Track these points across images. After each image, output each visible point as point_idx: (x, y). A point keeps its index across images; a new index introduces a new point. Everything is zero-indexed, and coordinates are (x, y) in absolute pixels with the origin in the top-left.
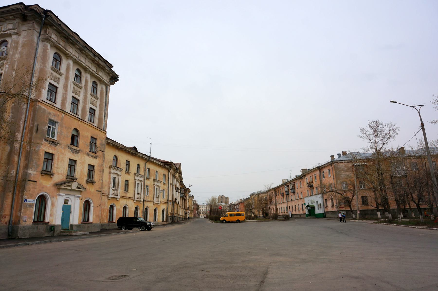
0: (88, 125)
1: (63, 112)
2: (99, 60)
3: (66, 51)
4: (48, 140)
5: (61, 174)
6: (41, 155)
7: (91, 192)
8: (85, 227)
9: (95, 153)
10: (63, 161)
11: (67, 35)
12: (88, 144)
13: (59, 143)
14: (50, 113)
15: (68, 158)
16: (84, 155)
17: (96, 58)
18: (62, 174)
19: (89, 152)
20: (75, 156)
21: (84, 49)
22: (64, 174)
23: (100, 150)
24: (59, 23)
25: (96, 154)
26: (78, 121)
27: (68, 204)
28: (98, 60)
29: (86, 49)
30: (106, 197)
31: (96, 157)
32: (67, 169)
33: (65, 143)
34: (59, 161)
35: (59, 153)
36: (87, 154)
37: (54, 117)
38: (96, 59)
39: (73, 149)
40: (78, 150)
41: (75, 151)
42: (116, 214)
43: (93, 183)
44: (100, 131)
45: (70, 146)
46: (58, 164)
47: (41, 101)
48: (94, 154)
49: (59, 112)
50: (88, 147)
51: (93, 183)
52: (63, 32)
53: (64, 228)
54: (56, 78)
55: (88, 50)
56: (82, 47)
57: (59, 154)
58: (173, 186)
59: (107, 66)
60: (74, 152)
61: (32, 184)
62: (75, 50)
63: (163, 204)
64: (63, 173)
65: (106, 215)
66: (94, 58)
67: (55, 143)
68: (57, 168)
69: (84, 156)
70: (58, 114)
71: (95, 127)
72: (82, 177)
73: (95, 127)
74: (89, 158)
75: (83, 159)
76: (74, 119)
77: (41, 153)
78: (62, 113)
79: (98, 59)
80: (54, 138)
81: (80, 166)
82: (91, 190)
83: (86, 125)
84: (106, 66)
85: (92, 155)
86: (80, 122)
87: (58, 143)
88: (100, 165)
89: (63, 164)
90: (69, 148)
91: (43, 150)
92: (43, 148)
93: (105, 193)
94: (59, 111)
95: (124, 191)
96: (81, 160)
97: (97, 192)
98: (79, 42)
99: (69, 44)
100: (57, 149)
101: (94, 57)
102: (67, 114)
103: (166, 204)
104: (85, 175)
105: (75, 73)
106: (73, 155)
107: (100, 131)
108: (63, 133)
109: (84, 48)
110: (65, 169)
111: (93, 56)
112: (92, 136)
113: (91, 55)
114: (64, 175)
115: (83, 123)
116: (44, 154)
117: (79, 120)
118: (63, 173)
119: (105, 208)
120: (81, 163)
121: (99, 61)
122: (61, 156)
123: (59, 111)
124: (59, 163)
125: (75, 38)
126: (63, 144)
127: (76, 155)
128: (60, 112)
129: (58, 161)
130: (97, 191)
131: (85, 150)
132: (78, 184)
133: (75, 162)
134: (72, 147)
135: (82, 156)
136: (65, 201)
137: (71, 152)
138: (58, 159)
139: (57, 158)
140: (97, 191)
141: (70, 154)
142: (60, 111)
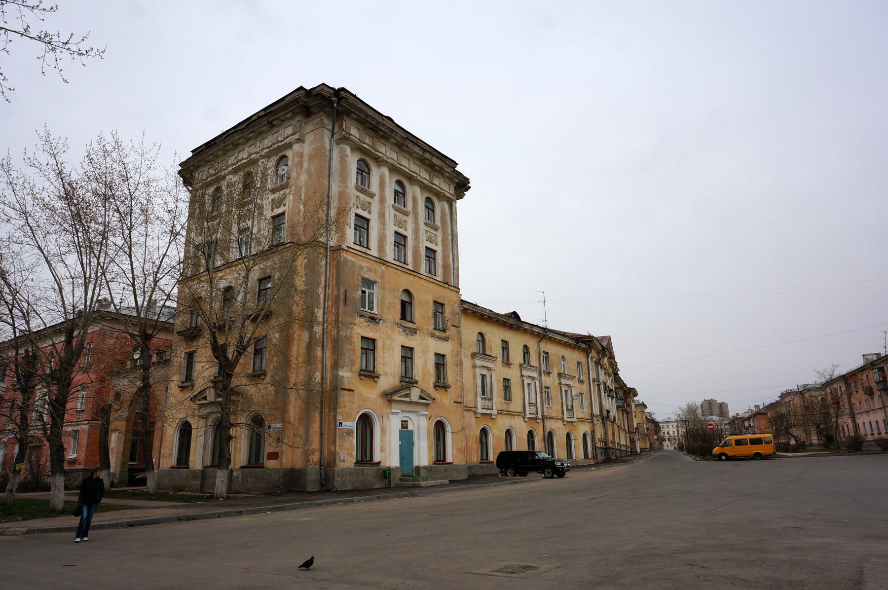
1: (382, 262)
3: (376, 153)
9: (444, 331)
14: (362, 268)
16: (425, 337)
20: (409, 340)
22: (396, 373)
23: (452, 325)
27: (408, 429)
29: (408, 141)
31: (446, 339)
34: (386, 351)
42: (493, 445)
46: (383, 357)
49: (376, 263)
52: (368, 119)
56: (401, 139)
57: (383, 338)
74: (435, 342)
78: (382, 265)
83: (422, 282)
89: (392, 358)
95: (503, 401)
97: (455, 404)
102: (389, 264)
106: (407, 338)
107: (449, 288)
114: (396, 377)
129: (384, 352)
130: (454, 402)
131: (425, 327)
136: (403, 423)
139: (381, 348)
140: (454, 402)
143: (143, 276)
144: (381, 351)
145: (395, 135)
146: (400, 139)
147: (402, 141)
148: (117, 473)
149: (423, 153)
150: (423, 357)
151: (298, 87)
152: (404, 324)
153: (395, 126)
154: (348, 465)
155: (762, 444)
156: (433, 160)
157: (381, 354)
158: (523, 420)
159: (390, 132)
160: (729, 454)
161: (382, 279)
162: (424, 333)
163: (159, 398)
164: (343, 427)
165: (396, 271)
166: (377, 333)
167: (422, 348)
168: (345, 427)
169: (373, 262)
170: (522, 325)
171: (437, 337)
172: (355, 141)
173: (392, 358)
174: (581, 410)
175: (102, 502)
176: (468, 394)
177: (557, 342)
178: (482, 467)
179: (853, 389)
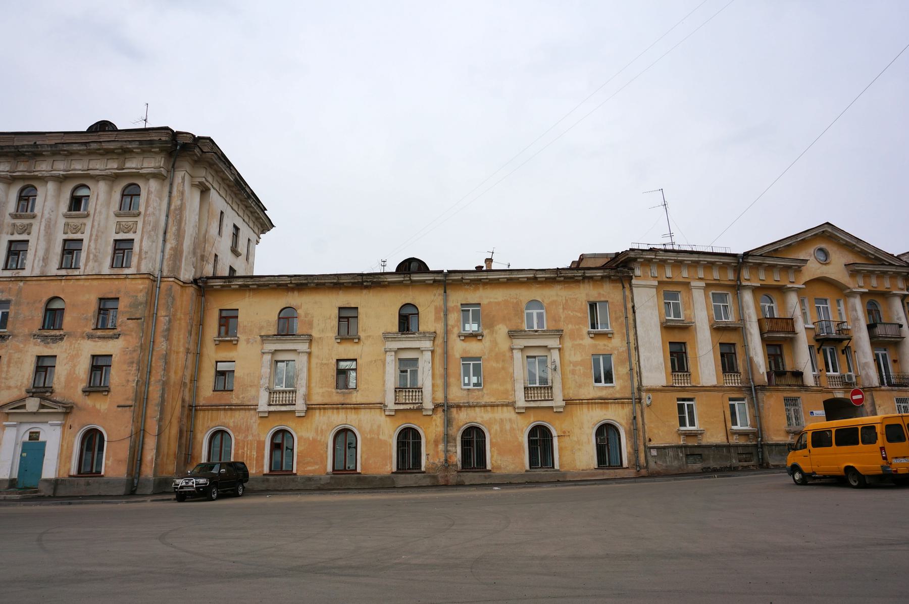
1: (19, 279)
2: (99, 144)
3: (32, 174)
7: (99, 411)
8: (78, 484)
10: (22, 363)
11: (13, 150)
12: (89, 315)
13: (10, 334)
16: (77, 340)
17: (90, 146)
19: (92, 331)
20: (51, 348)
21: (58, 149)
22: (24, 385)
23: (128, 319)
24: (30, 141)
26: (59, 281)
27: (38, 440)
28: (99, 146)
29: (60, 145)
30: (252, 412)
31: (117, 336)
32: (30, 376)
33: (27, 331)
34: (11, 365)
35: (11, 351)
38: (92, 147)
39: (47, 336)
41: (51, 339)
42: (298, 453)
43: (104, 390)
44: (127, 280)
46: (7, 371)
48: (110, 332)
50: (91, 320)
51: (104, 390)
52: (5, 150)
53: (28, 486)
54: (127, 227)
55: (65, 145)
56: (51, 147)
57: (10, 353)
59: (128, 143)
62: (142, 156)
63: (368, 410)
65: (255, 456)
66: (89, 148)
70: (10, 286)
71: (107, 277)
72: (72, 384)
73: (107, 277)
75: (74, 347)
76: (48, 282)
79: (95, 144)
82: (98, 406)
83: (81, 283)
84: (125, 143)
85: (103, 334)
87: (9, 336)
89: (20, 370)
93: (249, 403)
95: (334, 390)
96: (68, 352)
97: (120, 409)
98: (39, 146)
99: (35, 159)
100: (7, 346)
101: (86, 148)
102: (28, 279)
103: (628, 403)
104: (81, 378)
106: (46, 347)
108: (22, 315)
109: (56, 147)
110: (26, 376)
111: (84, 147)
113: (79, 148)
116: (719, 348)
118: (21, 385)
119: (250, 438)
120: (67, 357)
121: (102, 146)
122: (16, 355)
125: (27, 145)
126: (22, 334)
128: (14, 282)
129: (8, 366)
130: (118, 406)
131: (79, 330)
132: (468, 392)
133: (734, 346)
136: (31, 435)
138: (9, 362)
139: (5, 363)
140: (118, 406)
141: (37, 347)
144: (5, 366)
145: (42, 147)
146: (49, 149)
147: (54, 149)
149: (86, 146)
151: (88, 128)
152: (45, 333)
153: (63, 134)
155: (858, 443)
156: (104, 147)
157: (5, 369)
158: (514, 411)
159: (34, 148)
160: (806, 468)
161: (17, 296)
164: (815, 415)
165: (39, 282)
167: (69, 354)
168: (816, 415)
169: (7, 282)
170: (380, 278)
171: (98, 338)
172: (5, 176)
173: (20, 370)
174: (831, 373)
176: (249, 389)
177: (504, 283)
178: (268, 480)
179: (716, 275)
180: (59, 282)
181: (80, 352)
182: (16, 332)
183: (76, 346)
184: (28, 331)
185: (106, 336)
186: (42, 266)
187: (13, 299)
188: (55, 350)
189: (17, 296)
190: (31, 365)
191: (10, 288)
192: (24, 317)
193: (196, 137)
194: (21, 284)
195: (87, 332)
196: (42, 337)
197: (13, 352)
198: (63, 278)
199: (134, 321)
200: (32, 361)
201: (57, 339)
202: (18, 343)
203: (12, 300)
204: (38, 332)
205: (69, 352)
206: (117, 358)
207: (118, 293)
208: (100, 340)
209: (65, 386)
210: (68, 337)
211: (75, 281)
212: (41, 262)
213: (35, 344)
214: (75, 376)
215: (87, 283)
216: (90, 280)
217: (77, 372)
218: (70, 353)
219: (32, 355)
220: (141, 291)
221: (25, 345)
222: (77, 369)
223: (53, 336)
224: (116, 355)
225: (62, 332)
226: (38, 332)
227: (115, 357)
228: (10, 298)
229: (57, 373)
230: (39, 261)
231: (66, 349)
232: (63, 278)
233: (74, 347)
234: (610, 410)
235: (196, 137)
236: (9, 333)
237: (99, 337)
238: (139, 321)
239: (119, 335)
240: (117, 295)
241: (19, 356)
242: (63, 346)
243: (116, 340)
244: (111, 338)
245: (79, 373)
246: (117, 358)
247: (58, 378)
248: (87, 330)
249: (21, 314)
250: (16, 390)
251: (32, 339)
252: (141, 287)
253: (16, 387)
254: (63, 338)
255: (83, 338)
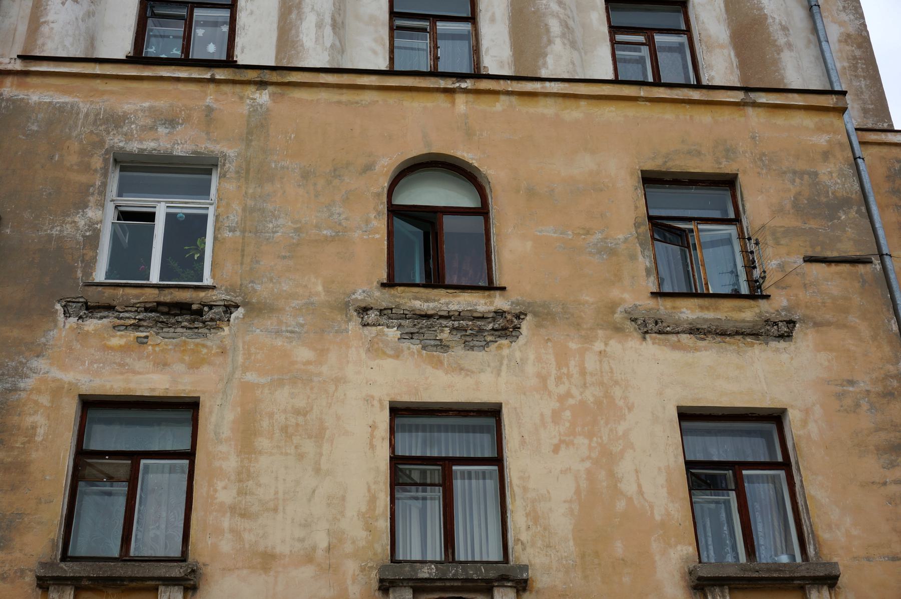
0: (569, 102)
4: (110, 308)
5: (309, 558)
6: (41, 431)
9: (756, 293)
10: (319, 435)
13: (238, 300)
14: (116, 121)
15: (368, 399)
16: (588, 339)
18: (320, 554)
19: (651, 303)
22: (348, 548)
23: (809, 260)
25: (763, 303)
27: (148, 280)
32: (373, 500)
33: (320, 288)
34: (263, 443)
35: (251, 377)
36: (630, 326)
37: (162, 130)
39: (428, 316)
40: (500, 313)
41: (453, 329)
44: (750, 111)
45: (384, 298)
46: (244, 475)
47: (18, 66)
48: (740, 310)
49: (212, 87)
57: (247, 388)
58: (379, 367)
60: (445, 335)
61: (387, 525)
64: (323, 544)
67: (200, 313)
68: (245, 515)
69: (599, 346)
70: (209, 100)
74: (677, 355)
75: (583, 372)
76: (392, 99)
77: (39, 419)
78: (252, 88)
80: (202, 281)
81: (556, 449)
85: (710, 315)
86: (460, 99)
87: (229, 308)
88: (864, 385)
89: (317, 471)
90: (372, 316)
91: (57, 390)
92: (56, 373)
94: (212, 80)
100: (223, 352)
105: (651, 218)
106: (439, 364)
107: (755, 104)
110: (356, 502)
112: (650, 166)
114: (351, 567)
115: (503, 98)
117: (446, 91)
118: (329, 549)
120: (556, 416)
123: (212, 80)
124: (264, 461)
126: (295, 303)
127: (476, 358)
131: (588, 297)
134: (417, 304)
135: (562, 358)
137: (406, 344)
139: (226, 432)
141: (389, 363)
142: (217, 77)
143: (218, 385)
148: (863, 106)
150: (581, 441)
154: (226, 329)
157: (231, 463)
162: (578, 326)
163: (251, 373)
166: (205, 369)
167: (562, 398)
173: (317, 471)
175: (419, 283)
180: (441, 101)
181: (617, 392)
182: (262, 290)
183: (591, 363)
184: (328, 291)
185: (730, 327)
186: (333, 46)
187: (231, 153)
188: (486, 378)
189: (248, 143)
190: (372, 447)
191: (209, 110)
192: (297, 231)
193: (212, 43)
194: (263, 97)
195: (628, 305)
196: (405, 317)
197: (263, 380)
198: (463, 85)
199: (834, 268)
200: (373, 427)
201: (481, 330)
202: (279, 342)
203: (225, 156)
204: (384, 298)
205: (562, 389)
206: (813, 428)
207: (727, 158)
208: (701, 344)
209: (583, 556)
210: (539, 326)
211: (514, 99)
212: (328, 30)
213: (375, 349)
214: (621, 505)
215: (576, 113)
216: (583, 103)
217: (629, 487)
218: (568, 395)
219: (368, 399)
220: (826, 155)
221: (322, 353)
222: (625, 467)
223: (460, 316)
224: (807, 411)
225: (499, 302)
226: (377, 294)
227: (805, 423)
228: (216, 148)
229: (525, 489)
230: (320, 25)
231: (543, 379)
232: (463, 85)
233: (583, 372)
234: (524, 560)
235: (212, 43)
236: (227, 292)
237: (695, 330)
238: (861, 268)
239: (791, 323)
240: (724, 163)
241: (300, 403)
242: (524, 360)
243: (782, 344)
244: (756, 335)
245: (641, 492)
246: (813, 428)
247: (534, 517)
248: (626, 296)
249: (277, 218)
250: (307, 572)
251: (354, 326)
252: (822, 140)
253: (309, 558)
254: (517, 328)
255: (618, 329)
